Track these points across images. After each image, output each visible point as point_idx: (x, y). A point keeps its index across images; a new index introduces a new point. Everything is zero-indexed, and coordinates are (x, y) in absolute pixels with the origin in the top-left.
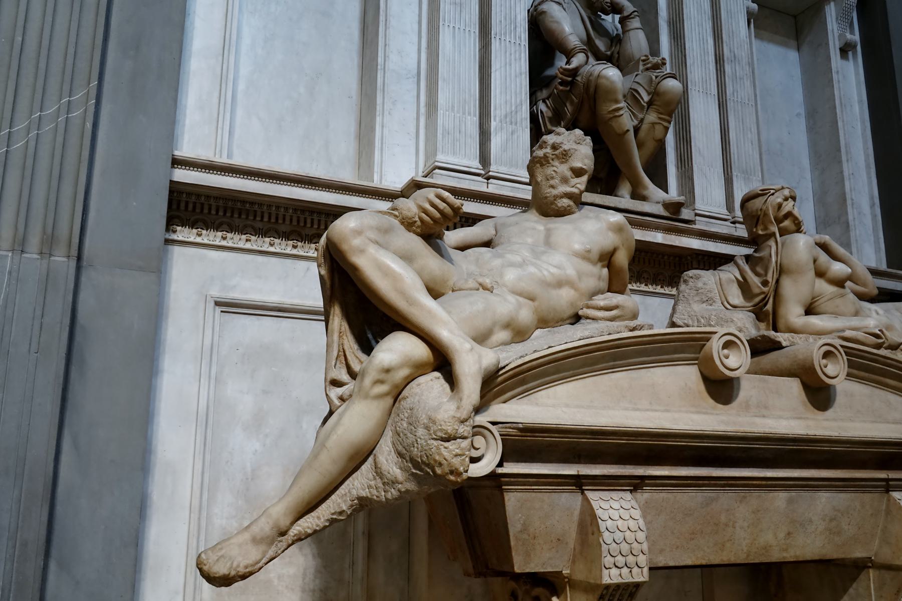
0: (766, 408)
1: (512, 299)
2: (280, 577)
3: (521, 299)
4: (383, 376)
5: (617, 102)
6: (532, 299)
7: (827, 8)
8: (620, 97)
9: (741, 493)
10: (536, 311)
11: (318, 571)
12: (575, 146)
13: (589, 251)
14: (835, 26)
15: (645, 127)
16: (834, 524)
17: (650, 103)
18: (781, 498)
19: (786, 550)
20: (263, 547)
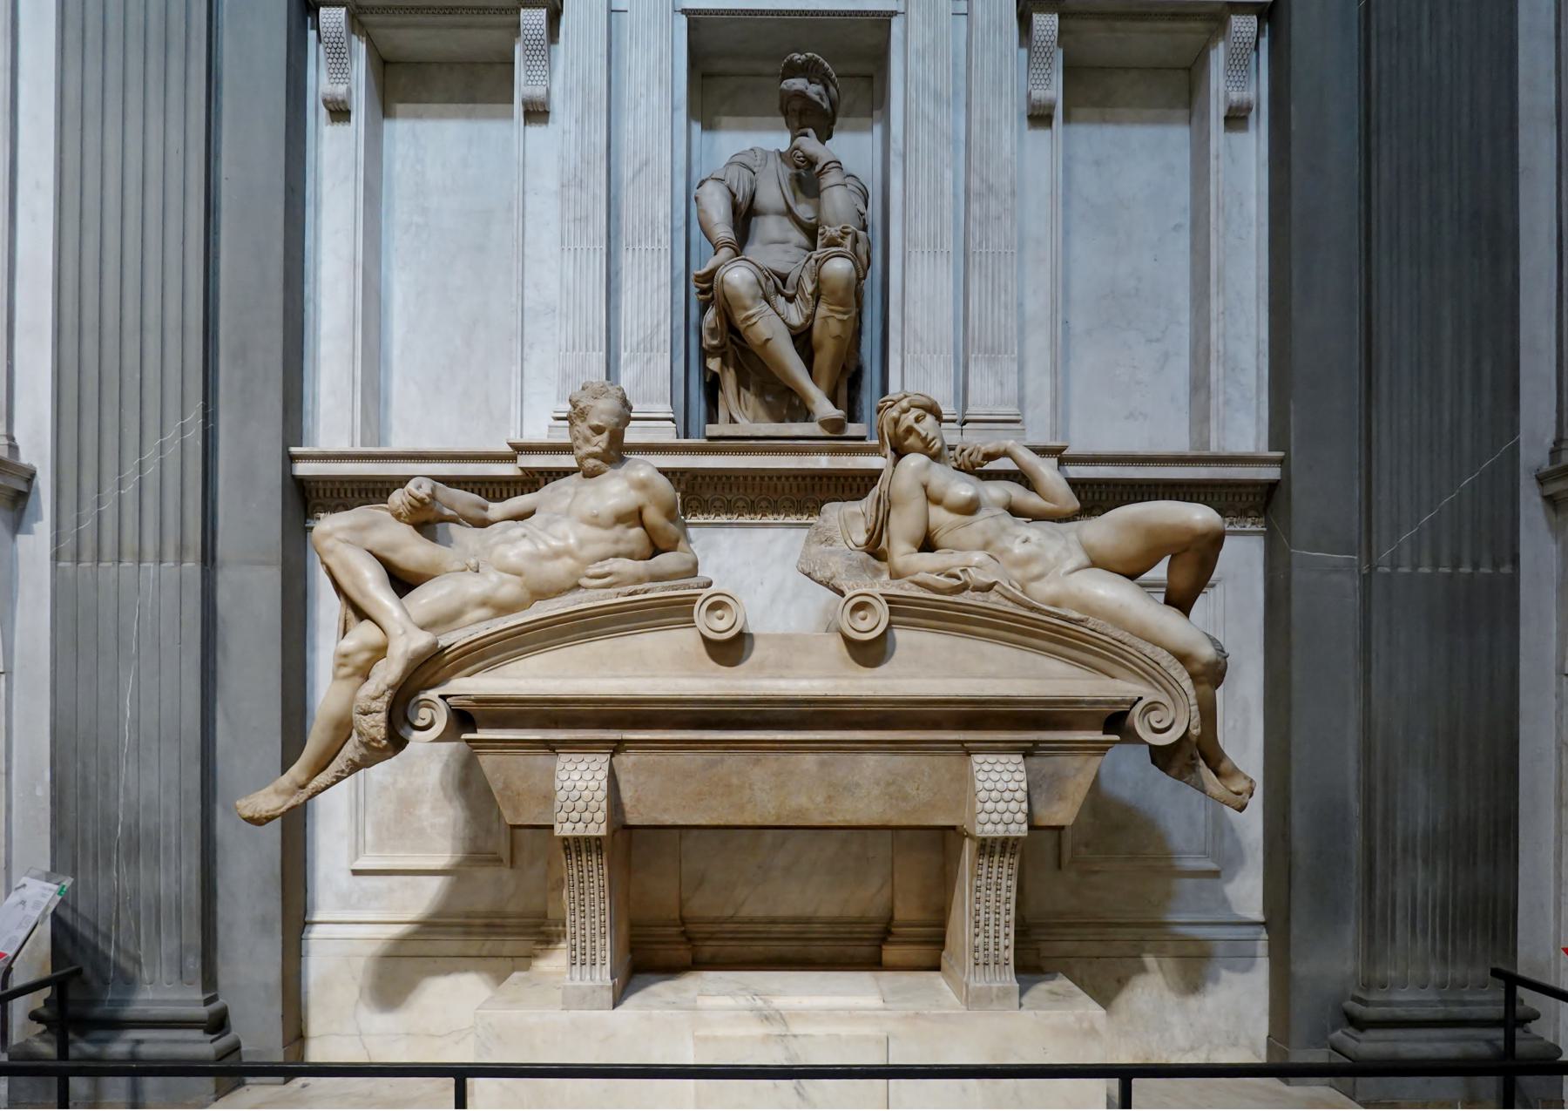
0: (787, 667)
1: (494, 577)
2: (433, 826)
3: (506, 576)
4: (342, 661)
5: (746, 309)
6: (519, 574)
7: (1212, 53)
8: (748, 302)
9: (753, 756)
10: (525, 585)
11: (467, 822)
12: (592, 403)
13: (597, 516)
14: (1222, 82)
15: (817, 323)
16: (892, 789)
17: (817, 296)
18: (809, 761)
19: (831, 813)
20: (284, 798)
